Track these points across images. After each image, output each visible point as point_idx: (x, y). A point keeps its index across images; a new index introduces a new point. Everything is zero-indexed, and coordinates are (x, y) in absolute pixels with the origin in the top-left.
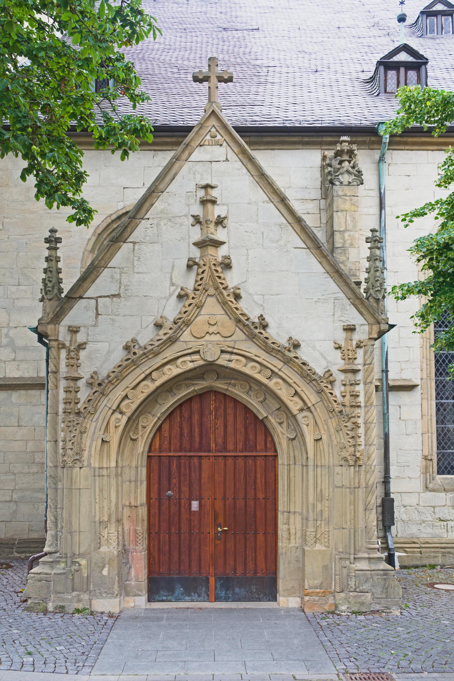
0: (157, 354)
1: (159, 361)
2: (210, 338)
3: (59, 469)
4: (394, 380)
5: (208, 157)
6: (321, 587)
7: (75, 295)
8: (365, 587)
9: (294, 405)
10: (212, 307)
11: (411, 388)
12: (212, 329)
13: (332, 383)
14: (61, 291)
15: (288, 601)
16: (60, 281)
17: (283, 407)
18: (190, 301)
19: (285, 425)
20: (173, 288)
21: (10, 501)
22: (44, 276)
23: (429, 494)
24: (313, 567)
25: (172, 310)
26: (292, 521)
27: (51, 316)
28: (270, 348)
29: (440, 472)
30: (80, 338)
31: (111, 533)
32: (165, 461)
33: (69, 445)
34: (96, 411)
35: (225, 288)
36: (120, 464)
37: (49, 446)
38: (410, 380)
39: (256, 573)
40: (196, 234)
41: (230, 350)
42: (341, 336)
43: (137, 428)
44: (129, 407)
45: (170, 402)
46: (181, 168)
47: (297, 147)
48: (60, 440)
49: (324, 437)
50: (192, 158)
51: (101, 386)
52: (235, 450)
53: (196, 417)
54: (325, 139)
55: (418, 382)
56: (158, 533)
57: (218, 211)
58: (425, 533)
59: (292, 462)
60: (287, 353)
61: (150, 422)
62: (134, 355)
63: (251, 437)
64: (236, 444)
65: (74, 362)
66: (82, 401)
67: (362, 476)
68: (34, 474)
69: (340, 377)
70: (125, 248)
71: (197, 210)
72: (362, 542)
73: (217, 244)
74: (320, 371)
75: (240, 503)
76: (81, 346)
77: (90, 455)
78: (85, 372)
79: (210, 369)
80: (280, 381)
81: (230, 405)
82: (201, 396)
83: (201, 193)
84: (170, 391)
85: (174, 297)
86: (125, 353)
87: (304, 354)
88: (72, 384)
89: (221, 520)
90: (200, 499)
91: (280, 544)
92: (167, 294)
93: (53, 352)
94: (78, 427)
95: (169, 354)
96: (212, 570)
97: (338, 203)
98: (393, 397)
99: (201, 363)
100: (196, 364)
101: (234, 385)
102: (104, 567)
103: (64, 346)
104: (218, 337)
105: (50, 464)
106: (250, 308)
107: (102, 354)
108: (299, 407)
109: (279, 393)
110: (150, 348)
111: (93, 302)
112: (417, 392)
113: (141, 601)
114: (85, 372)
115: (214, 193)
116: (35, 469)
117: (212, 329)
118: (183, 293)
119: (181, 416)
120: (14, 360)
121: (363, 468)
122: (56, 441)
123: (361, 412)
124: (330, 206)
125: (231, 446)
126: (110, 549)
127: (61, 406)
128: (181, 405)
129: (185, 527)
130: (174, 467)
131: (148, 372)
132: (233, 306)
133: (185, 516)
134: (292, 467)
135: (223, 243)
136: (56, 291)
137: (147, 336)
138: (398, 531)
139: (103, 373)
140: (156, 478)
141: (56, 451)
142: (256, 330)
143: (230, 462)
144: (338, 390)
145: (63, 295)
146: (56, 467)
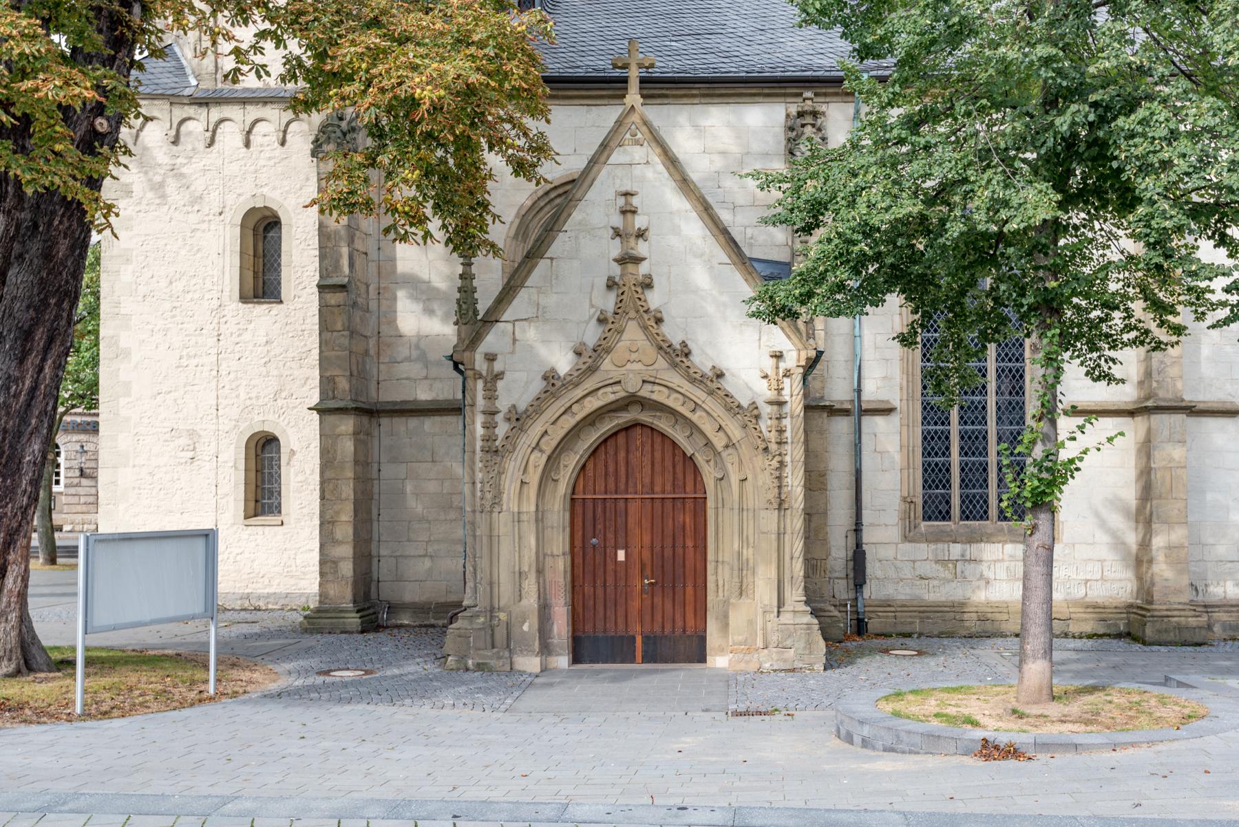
0: (577, 385)
1: (579, 393)
3: (478, 514)
4: (868, 401)
6: (745, 643)
7: (491, 319)
8: (788, 643)
9: (719, 441)
10: (633, 333)
11: (888, 411)
12: (634, 356)
13: (757, 417)
14: (476, 312)
15: (719, 661)
16: (475, 302)
17: (708, 443)
18: (610, 326)
19: (712, 463)
20: (593, 310)
21: (425, 556)
22: (458, 295)
23: (908, 546)
26: (720, 571)
27: (467, 342)
29: (927, 517)
30: (498, 366)
32: (590, 505)
33: (487, 488)
34: (514, 449)
35: (646, 312)
36: (540, 509)
37: (467, 489)
38: (888, 402)
39: (684, 631)
40: (615, 249)
41: (652, 379)
43: (558, 468)
44: (549, 445)
45: (592, 438)
46: (599, 171)
47: (757, 99)
48: (478, 481)
49: (750, 477)
50: (611, 160)
51: (519, 420)
52: (663, 492)
53: (622, 455)
54: (789, 91)
55: (896, 403)
56: (582, 586)
57: (639, 222)
58: (901, 593)
59: (720, 505)
60: (709, 383)
61: (571, 462)
63: (680, 476)
64: (664, 485)
65: (491, 395)
66: (500, 438)
67: (788, 521)
68: (451, 521)
69: (766, 410)
70: (543, 265)
71: (617, 221)
73: (637, 260)
74: (745, 404)
75: (668, 552)
76: (499, 376)
77: (509, 499)
79: (633, 400)
80: (704, 414)
81: (658, 440)
82: (628, 429)
83: (621, 201)
84: (593, 424)
85: (594, 321)
86: (545, 383)
87: (728, 384)
88: (489, 418)
89: (648, 572)
90: (626, 548)
91: (708, 598)
92: (587, 317)
93: (470, 382)
94: (496, 467)
96: (638, 629)
98: (867, 421)
99: (623, 394)
100: (618, 396)
101: (660, 418)
102: (524, 622)
103: (481, 376)
104: (638, 366)
105: (468, 509)
106: (673, 333)
108: (723, 443)
109: (703, 427)
110: (569, 378)
111: (509, 326)
112: (895, 419)
113: (562, 661)
114: (503, 404)
115: (635, 201)
116: (452, 515)
117: (634, 356)
118: (602, 317)
119: (606, 453)
120: (426, 378)
121: (788, 512)
122: (474, 483)
123: (788, 447)
125: (657, 488)
126: (531, 601)
127: (479, 444)
128: (605, 441)
130: (599, 510)
131: (568, 405)
132: (654, 331)
133: (610, 567)
134: (720, 510)
135: (644, 259)
136: (471, 313)
138: (872, 591)
139: (522, 406)
140: (581, 524)
141: (474, 495)
142: (679, 355)
143: (658, 504)
144: (763, 425)
145: (479, 317)
146: (474, 511)
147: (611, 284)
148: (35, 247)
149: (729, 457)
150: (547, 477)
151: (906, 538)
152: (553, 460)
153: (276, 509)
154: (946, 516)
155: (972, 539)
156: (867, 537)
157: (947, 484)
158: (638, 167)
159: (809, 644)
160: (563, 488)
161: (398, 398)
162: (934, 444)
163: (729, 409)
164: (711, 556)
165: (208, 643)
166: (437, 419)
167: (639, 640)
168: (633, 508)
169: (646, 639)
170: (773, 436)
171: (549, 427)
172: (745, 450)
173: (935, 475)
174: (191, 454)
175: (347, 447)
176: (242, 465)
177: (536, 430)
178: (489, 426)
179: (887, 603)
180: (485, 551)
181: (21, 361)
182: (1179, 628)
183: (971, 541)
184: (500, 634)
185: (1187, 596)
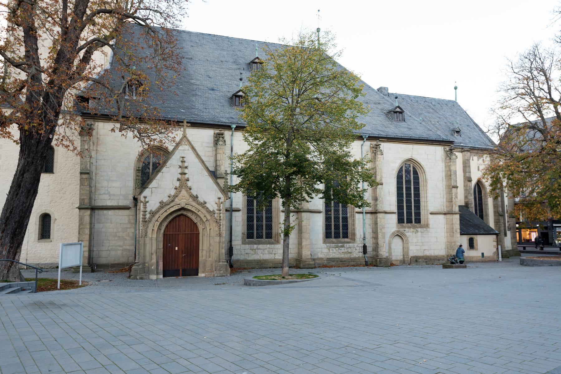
1: (169, 207)
2: (183, 200)
5: (183, 149)
9: (204, 219)
11: (239, 210)
15: (201, 275)
17: (201, 219)
23: (244, 245)
24: (208, 264)
25: (173, 192)
30: (147, 200)
31: (154, 257)
42: (217, 200)
44: (160, 220)
51: (153, 214)
53: (177, 223)
55: (241, 209)
58: (241, 258)
62: (163, 205)
69: (217, 212)
71: (180, 164)
72: (221, 258)
73: (185, 174)
74: (211, 210)
76: (148, 202)
79: (183, 209)
83: (181, 159)
87: (207, 205)
97: (219, 151)
98: (234, 213)
104: (185, 200)
106: (194, 192)
107: (153, 205)
112: (240, 213)
113: (161, 276)
114: (148, 209)
115: (185, 159)
116: (116, 238)
123: (221, 221)
124: (216, 150)
126: (154, 261)
127: (141, 220)
129: (173, 255)
137: (166, 199)
138: (234, 257)
139: (153, 210)
142: (195, 198)
144: (216, 215)
147: (178, 180)
148: (33, 168)
149: (207, 224)
150: (159, 229)
151: (243, 243)
152: (161, 224)
153: (49, 237)
154: (253, 238)
155: (259, 243)
156: (233, 243)
158: (184, 151)
159: (226, 270)
160: (162, 231)
161: (101, 205)
162: (250, 219)
164: (200, 248)
165: (82, 272)
166: (113, 211)
167: (181, 270)
168: (180, 236)
169: (183, 270)
170: (218, 218)
171: (162, 215)
172: (211, 221)
173: (250, 227)
175: (87, 219)
176: (38, 223)
177: (157, 216)
178: (144, 215)
179: (238, 261)
180: (142, 248)
181: (27, 198)
182: (308, 264)
183: (259, 244)
184: (146, 269)
185: (310, 257)
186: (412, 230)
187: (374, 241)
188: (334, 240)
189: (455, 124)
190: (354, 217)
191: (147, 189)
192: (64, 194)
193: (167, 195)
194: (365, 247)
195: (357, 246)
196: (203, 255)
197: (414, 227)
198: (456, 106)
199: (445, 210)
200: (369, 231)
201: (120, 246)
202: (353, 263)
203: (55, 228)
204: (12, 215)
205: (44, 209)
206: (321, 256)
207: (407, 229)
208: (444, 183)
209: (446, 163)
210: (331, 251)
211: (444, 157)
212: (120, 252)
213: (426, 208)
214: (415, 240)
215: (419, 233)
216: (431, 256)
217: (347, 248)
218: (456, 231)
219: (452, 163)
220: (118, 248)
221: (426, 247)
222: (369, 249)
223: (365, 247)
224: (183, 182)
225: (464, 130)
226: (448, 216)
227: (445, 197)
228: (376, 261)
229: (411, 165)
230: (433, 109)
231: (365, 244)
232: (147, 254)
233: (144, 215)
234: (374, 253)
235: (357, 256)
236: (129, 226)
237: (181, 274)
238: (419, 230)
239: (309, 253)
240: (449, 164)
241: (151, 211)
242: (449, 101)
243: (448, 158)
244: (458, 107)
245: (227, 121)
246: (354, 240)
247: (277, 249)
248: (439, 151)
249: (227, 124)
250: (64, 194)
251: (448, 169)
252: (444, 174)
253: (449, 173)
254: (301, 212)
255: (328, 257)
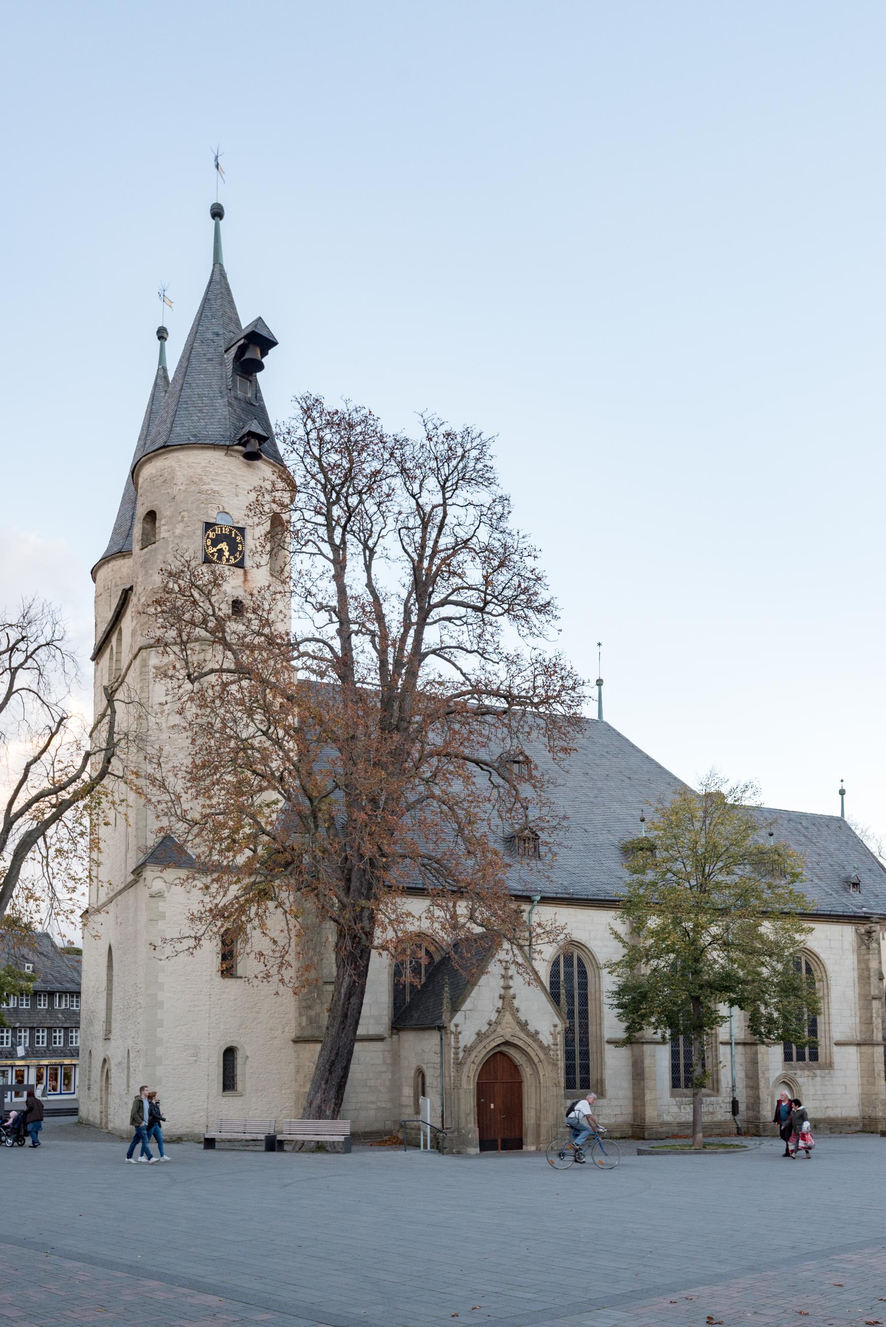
2: (508, 1030)
9: (536, 1060)
10: (508, 1017)
28: (528, 1033)
30: (459, 1029)
42: (552, 1029)
51: (468, 1050)
69: (552, 1047)
74: (546, 1045)
76: (460, 1033)
78: (462, 1045)
79: (507, 1043)
87: (540, 1037)
95: (492, 1037)
106: (522, 1017)
107: (467, 1037)
114: (462, 1045)
127: (452, 1061)
142: (523, 1026)
157: (574, 1073)
163: (540, 1047)
171: (480, 1055)
174: (195, 1058)
178: (456, 1054)
182: (656, 1133)
186: (806, 1073)
187: (751, 1093)
188: (685, 1091)
189: (849, 868)
190: (716, 1051)
191: (459, 1013)
192: (258, 1012)
193: (485, 1021)
194: (735, 1104)
195: (723, 1102)
196: (529, 1117)
197: (810, 1068)
198: (844, 828)
199: (858, 1038)
200: (740, 1074)
201: (373, 1103)
202: (717, 1131)
203: (243, 1071)
204: (339, 1058)
205: (229, 1039)
206: (667, 1118)
207: (798, 1072)
208: (857, 990)
209: (859, 955)
210: (683, 1111)
211: (855, 945)
212: (372, 1113)
213: (827, 1035)
214: (811, 1091)
215: (818, 1079)
216: (837, 1119)
217: (708, 1105)
218: (879, 1075)
219: (871, 956)
220: (370, 1105)
221: (829, 1103)
222: (742, 1107)
223: (735, 1104)
224: (507, 999)
225: (866, 880)
226: (865, 1049)
227: (858, 1014)
228: (757, 1127)
229: (803, 959)
230: (805, 836)
231: (734, 1098)
232: (462, 1115)
233: (456, 1054)
234: (751, 1113)
235: (722, 1119)
236: (384, 1068)
237: (499, 1147)
238: (818, 1072)
239: (656, 1113)
240: (866, 957)
241: (465, 1047)
242: (832, 818)
243: (864, 947)
244: (234, 316)
245: (519, 887)
246: (718, 1090)
247: (602, 1106)
248: (847, 933)
249: (524, 894)
250: (258, 1012)
251: (863, 966)
252: (856, 974)
253: (866, 973)
254: (643, 1043)
255: (678, 1120)
